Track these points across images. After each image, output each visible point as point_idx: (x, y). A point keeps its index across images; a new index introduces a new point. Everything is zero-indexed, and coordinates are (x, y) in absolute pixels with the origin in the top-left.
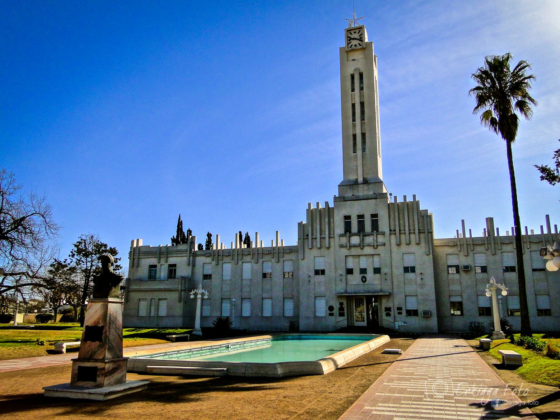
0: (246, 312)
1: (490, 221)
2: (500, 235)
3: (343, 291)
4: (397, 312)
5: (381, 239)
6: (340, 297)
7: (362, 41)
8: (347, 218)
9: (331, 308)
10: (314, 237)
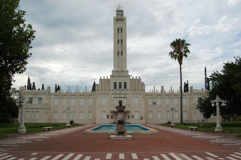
1: (162, 87)
2: (166, 92)
5: (127, 92)
7: (122, 16)
8: (115, 83)
9: (108, 116)
10: (102, 89)
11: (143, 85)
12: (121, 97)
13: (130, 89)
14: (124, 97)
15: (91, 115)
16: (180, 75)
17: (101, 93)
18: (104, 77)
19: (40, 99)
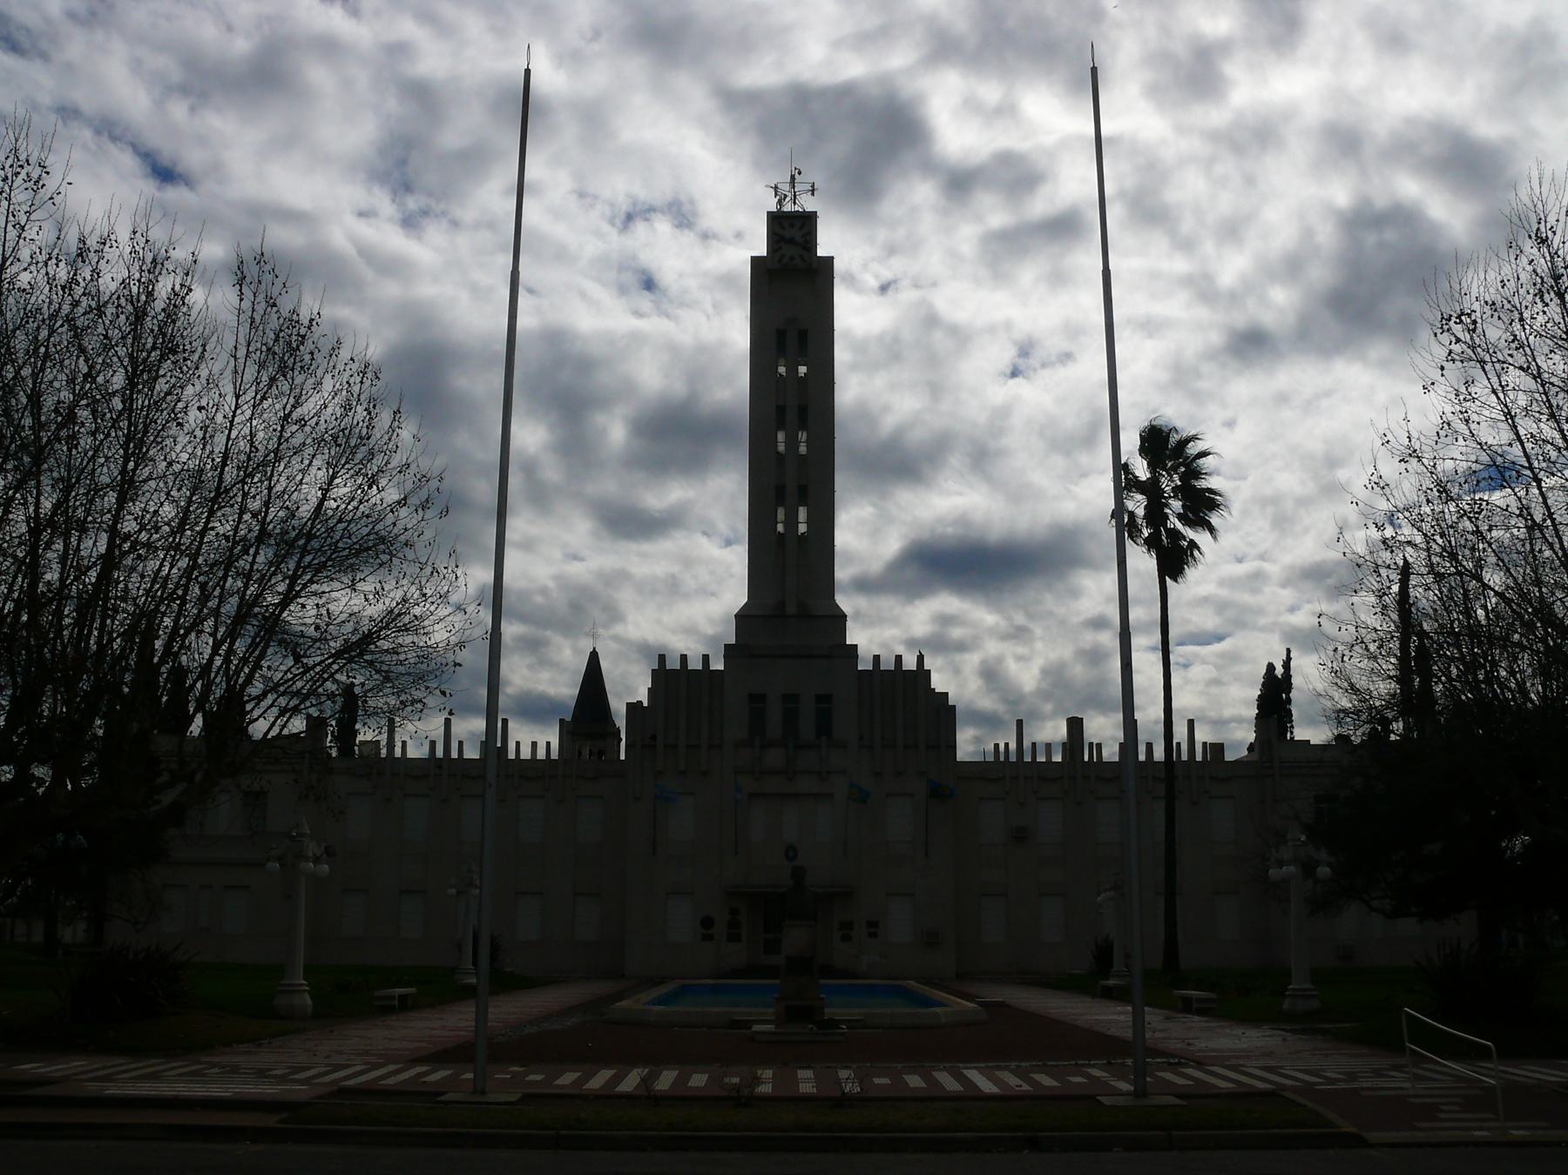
9: (707, 922)
11: (942, 713)
16: (1158, 636)
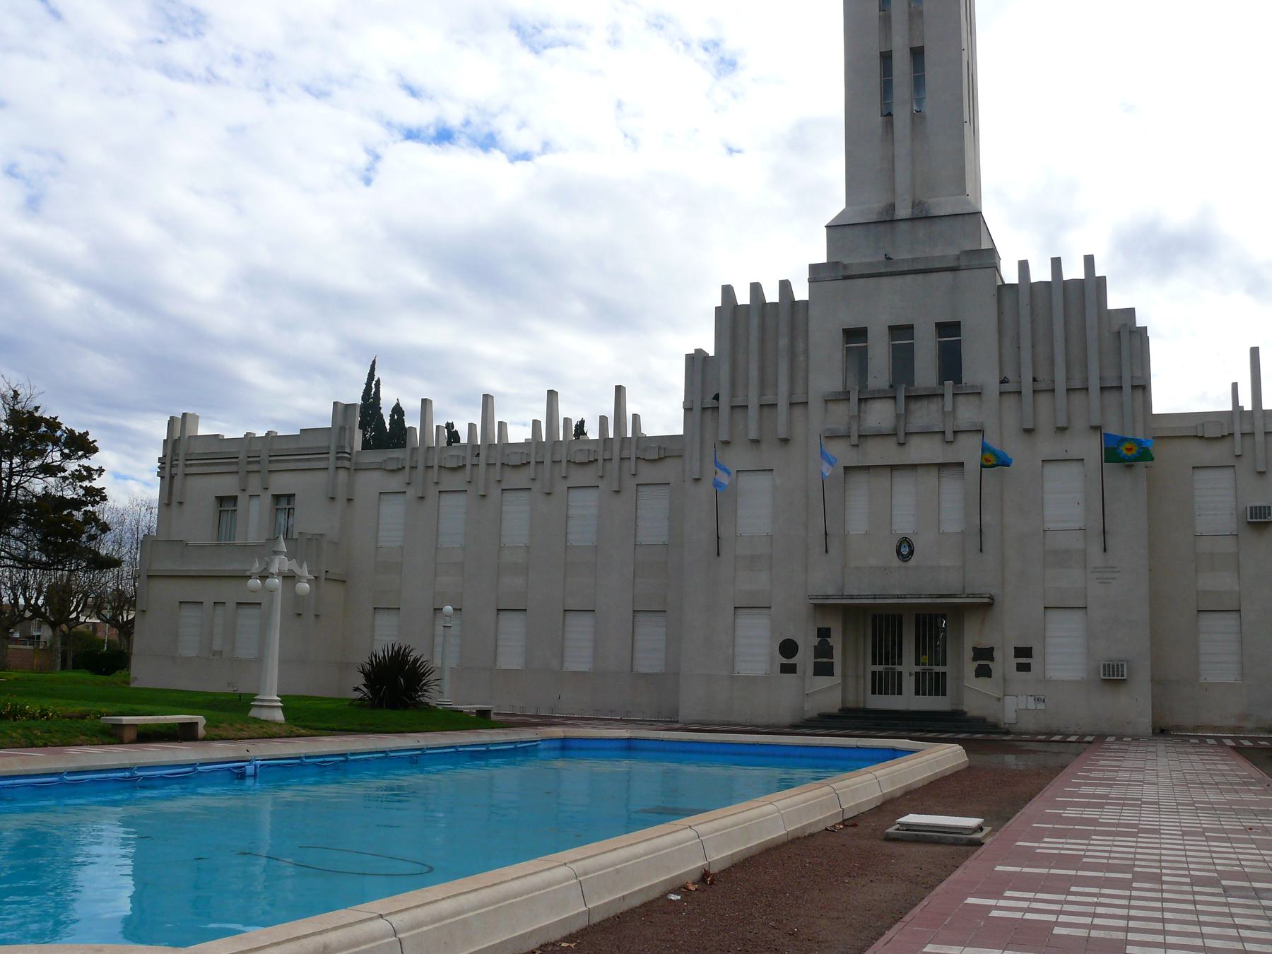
0: (511, 657)
3: (830, 592)
4: (1014, 662)
5: (967, 413)
6: (821, 608)
9: (788, 648)
11: (1128, 339)
12: (914, 467)
13: (993, 386)
14: (941, 466)
15: (652, 637)
17: (1062, 423)
18: (1056, 263)
19: (284, 501)
